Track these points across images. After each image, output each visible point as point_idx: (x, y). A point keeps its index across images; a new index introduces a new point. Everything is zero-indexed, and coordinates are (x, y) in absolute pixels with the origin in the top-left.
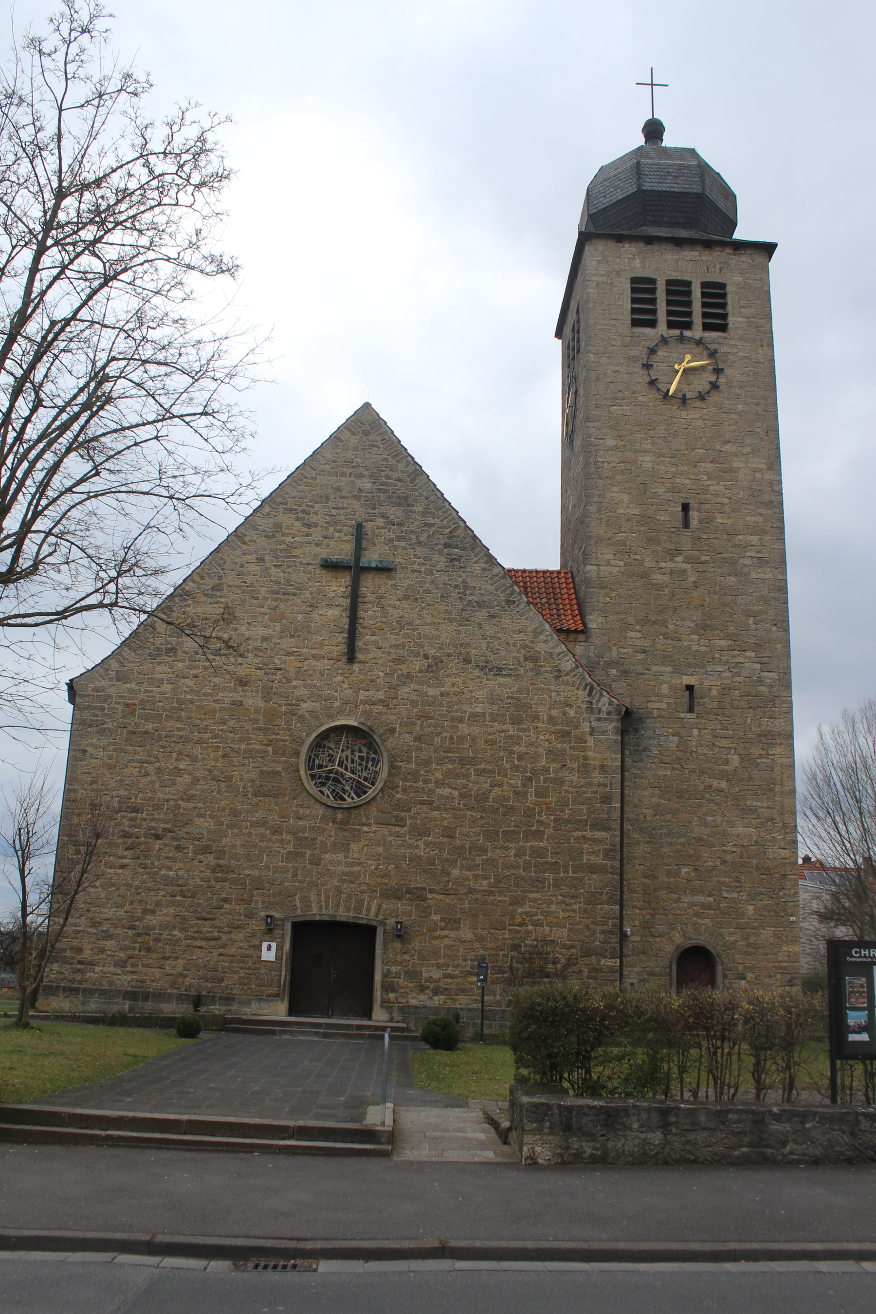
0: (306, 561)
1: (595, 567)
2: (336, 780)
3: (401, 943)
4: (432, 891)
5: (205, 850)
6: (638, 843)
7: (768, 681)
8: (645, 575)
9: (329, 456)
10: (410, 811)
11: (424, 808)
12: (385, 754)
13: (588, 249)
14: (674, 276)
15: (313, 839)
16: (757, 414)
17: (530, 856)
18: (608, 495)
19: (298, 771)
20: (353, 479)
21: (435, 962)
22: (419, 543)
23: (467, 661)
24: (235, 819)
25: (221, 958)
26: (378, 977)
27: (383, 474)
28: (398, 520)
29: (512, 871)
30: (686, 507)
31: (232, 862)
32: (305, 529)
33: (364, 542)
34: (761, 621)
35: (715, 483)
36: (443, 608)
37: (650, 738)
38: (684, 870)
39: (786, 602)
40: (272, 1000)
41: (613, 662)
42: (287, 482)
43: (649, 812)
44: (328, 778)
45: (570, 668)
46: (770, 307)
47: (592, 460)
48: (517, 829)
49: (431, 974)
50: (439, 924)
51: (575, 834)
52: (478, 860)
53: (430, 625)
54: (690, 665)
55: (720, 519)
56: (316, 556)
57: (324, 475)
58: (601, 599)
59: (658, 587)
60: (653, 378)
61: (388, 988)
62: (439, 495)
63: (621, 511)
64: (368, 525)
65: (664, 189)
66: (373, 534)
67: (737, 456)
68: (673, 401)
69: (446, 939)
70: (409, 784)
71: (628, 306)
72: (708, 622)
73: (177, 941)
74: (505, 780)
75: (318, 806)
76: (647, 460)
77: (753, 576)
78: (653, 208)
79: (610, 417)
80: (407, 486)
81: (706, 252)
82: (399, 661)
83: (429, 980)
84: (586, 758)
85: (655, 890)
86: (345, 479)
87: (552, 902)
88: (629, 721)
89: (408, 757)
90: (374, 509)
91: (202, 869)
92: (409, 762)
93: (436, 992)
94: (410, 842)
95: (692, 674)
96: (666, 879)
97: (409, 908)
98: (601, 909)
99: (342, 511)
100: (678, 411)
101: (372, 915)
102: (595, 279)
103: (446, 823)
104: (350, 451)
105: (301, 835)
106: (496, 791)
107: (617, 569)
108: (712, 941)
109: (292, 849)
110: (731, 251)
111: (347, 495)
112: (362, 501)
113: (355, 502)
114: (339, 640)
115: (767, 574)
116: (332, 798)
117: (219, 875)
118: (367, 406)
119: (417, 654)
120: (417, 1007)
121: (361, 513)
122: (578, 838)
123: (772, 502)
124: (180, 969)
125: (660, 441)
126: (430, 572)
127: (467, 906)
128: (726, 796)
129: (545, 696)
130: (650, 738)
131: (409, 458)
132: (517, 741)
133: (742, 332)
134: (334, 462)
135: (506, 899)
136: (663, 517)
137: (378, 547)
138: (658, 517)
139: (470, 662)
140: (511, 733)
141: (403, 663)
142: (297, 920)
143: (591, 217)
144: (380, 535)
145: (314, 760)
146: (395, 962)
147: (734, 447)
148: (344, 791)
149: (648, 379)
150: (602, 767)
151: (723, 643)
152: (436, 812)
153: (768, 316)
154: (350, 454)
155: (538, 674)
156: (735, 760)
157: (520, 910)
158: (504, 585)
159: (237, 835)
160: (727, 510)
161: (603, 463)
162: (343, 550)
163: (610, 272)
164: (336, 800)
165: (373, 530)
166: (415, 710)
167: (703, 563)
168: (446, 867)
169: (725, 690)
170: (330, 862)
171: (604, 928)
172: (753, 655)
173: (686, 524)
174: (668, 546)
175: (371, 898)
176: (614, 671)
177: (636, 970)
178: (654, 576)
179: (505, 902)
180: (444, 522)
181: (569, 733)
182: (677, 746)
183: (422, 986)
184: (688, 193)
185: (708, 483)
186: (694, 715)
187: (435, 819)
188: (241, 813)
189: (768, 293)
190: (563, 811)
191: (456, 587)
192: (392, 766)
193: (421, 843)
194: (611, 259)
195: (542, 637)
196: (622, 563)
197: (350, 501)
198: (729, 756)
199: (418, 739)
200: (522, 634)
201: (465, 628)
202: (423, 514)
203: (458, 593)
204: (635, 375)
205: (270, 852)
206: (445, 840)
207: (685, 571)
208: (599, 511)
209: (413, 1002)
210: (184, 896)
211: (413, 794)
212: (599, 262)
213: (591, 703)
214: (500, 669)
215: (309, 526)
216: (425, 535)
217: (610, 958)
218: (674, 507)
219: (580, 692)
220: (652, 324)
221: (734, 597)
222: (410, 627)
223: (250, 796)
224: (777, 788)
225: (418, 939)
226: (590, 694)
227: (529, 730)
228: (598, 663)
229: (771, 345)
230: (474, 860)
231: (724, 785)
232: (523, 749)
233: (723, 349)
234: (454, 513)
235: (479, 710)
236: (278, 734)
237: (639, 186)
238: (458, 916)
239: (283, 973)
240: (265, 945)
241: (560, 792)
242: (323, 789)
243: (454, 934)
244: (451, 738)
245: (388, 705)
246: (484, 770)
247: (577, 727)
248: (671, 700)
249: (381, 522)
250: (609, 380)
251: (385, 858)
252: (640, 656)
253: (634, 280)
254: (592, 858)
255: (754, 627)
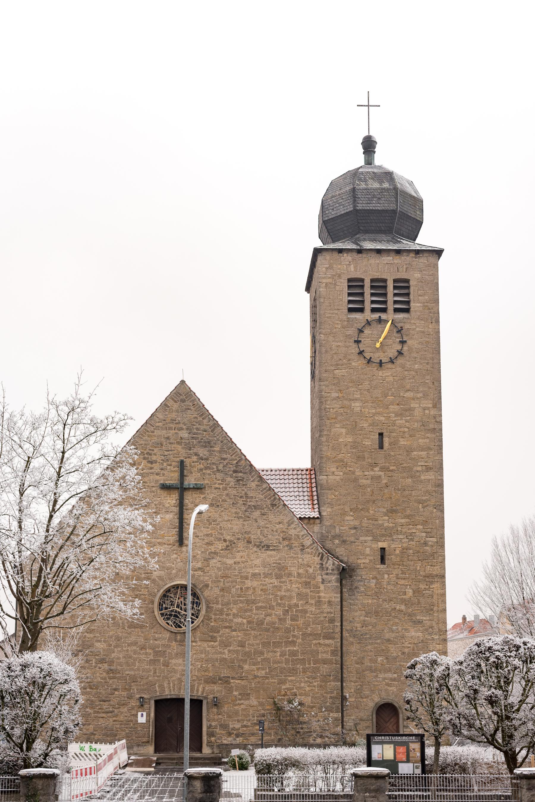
0: (151, 485)
1: (325, 477)
2: (176, 616)
3: (217, 709)
4: (233, 678)
5: (102, 661)
6: (352, 643)
7: (430, 543)
8: (356, 480)
9: (161, 417)
10: (219, 632)
11: (227, 630)
12: (203, 600)
13: (320, 258)
14: (377, 275)
15: (164, 652)
16: (427, 370)
17: (289, 655)
18: (333, 430)
19: (154, 612)
20: (176, 431)
21: (236, 719)
22: (218, 470)
23: (249, 542)
24: (118, 642)
25: (115, 723)
26: (204, 729)
27: (195, 427)
28: (205, 457)
29: (279, 665)
30: (381, 435)
31: (118, 667)
32: (149, 465)
33: (185, 471)
34: (427, 506)
35: (400, 418)
36: (234, 510)
37: (359, 581)
38: (380, 659)
39: (442, 493)
40: (145, 745)
41: (336, 535)
42: (136, 435)
43: (359, 625)
44: (171, 615)
45: (309, 544)
46: (438, 295)
47: (323, 407)
48: (281, 641)
49: (235, 726)
50: (238, 697)
51: (314, 642)
52: (259, 659)
53: (227, 521)
54: (383, 535)
55: (402, 442)
56: (157, 481)
57: (159, 429)
58: (329, 497)
59: (364, 487)
60: (361, 349)
61: (211, 734)
62: (229, 439)
63: (341, 440)
64: (187, 461)
65: (371, 208)
66: (191, 466)
67: (413, 399)
68: (374, 365)
69: (242, 705)
70: (218, 617)
71: (346, 298)
72: (394, 508)
73: (89, 714)
74: (273, 612)
75: (166, 632)
76: (357, 406)
77: (422, 478)
78: (364, 221)
79: (334, 378)
80: (209, 434)
81: (397, 257)
82: (208, 544)
83: (233, 729)
84: (319, 597)
85: (363, 671)
86: (171, 431)
87: (302, 682)
88: (346, 573)
89: (217, 601)
90: (190, 450)
91: (101, 672)
92: (217, 603)
93: (237, 736)
94: (220, 650)
95: (384, 541)
96: (369, 664)
97: (220, 688)
98: (330, 685)
99: (171, 452)
100: (377, 371)
101: (200, 694)
102: (324, 281)
103: (240, 639)
104: (174, 413)
105: (157, 649)
106: (268, 618)
107: (339, 477)
108: (396, 700)
109: (152, 658)
110: (414, 255)
111: (173, 441)
112: (183, 446)
113: (178, 446)
114: (173, 533)
115: (431, 476)
116: (174, 627)
117: (111, 675)
118: (183, 382)
119: (220, 539)
120: (227, 745)
121: (181, 452)
122: (316, 644)
123: (435, 429)
124: (91, 730)
125: (366, 392)
126: (225, 489)
127: (253, 686)
128: (405, 614)
129: (295, 561)
130: (359, 581)
131: (210, 416)
132: (279, 588)
133: (419, 314)
134: (164, 420)
135: (276, 681)
136: (367, 443)
137: (194, 474)
138: (364, 443)
139: (251, 542)
140: (276, 584)
141: (212, 545)
142: (157, 698)
143: (324, 222)
144: (195, 466)
145: (162, 605)
146: (214, 720)
147: (412, 394)
148: (181, 622)
149: (358, 351)
150: (329, 602)
151: (403, 521)
152: (234, 633)
153: (436, 301)
154: (174, 415)
155: (291, 548)
156: (410, 592)
157: (284, 687)
158: (270, 495)
159: (120, 652)
160: (407, 436)
161: (330, 409)
162: (173, 478)
163: (335, 276)
164: (176, 628)
165: (190, 463)
166: (220, 573)
167: (392, 471)
168: (241, 664)
169: (404, 550)
170: (175, 665)
171: (332, 695)
172: (421, 527)
173: (381, 447)
174: (370, 460)
175: (199, 684)
176: (337, 541)
177: (352, 718)
178: (361, 481)
179: (275, 682)
180: (233, 457)
181: (309, 583)
182: (375, 585)
183: (229, 733)
184: (387, 211)
185: (396, 418)
186: (385, 566)
187: (234, 637)
188: (121, 638)
189: (437, 284)
190: (307, 629)
191: (241, 497)
192: (208, 607)
193: (226, 651)
194: (335, 266)
195: (293, 526)
196: (341, 473)
197: (175, 445)
198: (406, 590)
199: (222, 590)
200: (281, 524)
201: (247, 522)
202: (220, 452)
203: (243, 501)
204: (350, 348)
205: (140, 660)
206: (240, 648)
207: (380, 476)
208: (327, 441)
209: (225, 742)
210: (92, 689)
211: (221, 623)
212: (327, 268)
213: (322, 564)
214: (268, 546)
215: (151, 463)
216: (221, 465)
217: (336, 712)
218: (374, 435)
219: (316, 558)
220: (361, 310)
221: (410, 492)
222: (215, 523)
223: (126, 628)
224: (435, 608)
225: (227, 706)
226: (321, 559)
227: (286, 583)
228: (328, 537)
229: (438, 321)
230: (257, 659)
231: (403, 607)
232: (283, 594)
233: (407, 326)
234: (239, 451)
235: (257, 571)
236: (140, 591)
237: (355, 206)
238: (249, 692)
239: (151, 729)
240: (140, 714)
241: (305, 618)
242: (168, 622)
243: (247, 702)
244: (241, 589)
245: (204, 571)
246: (261, 607)
247: (314, 579)
248: (372, 558)
249: (195, 458)
250: (334, 352)
251: (206, 661)
252: (353, 531)
253: (349, 280)
254: (324, 655)
255: (422, 510)
